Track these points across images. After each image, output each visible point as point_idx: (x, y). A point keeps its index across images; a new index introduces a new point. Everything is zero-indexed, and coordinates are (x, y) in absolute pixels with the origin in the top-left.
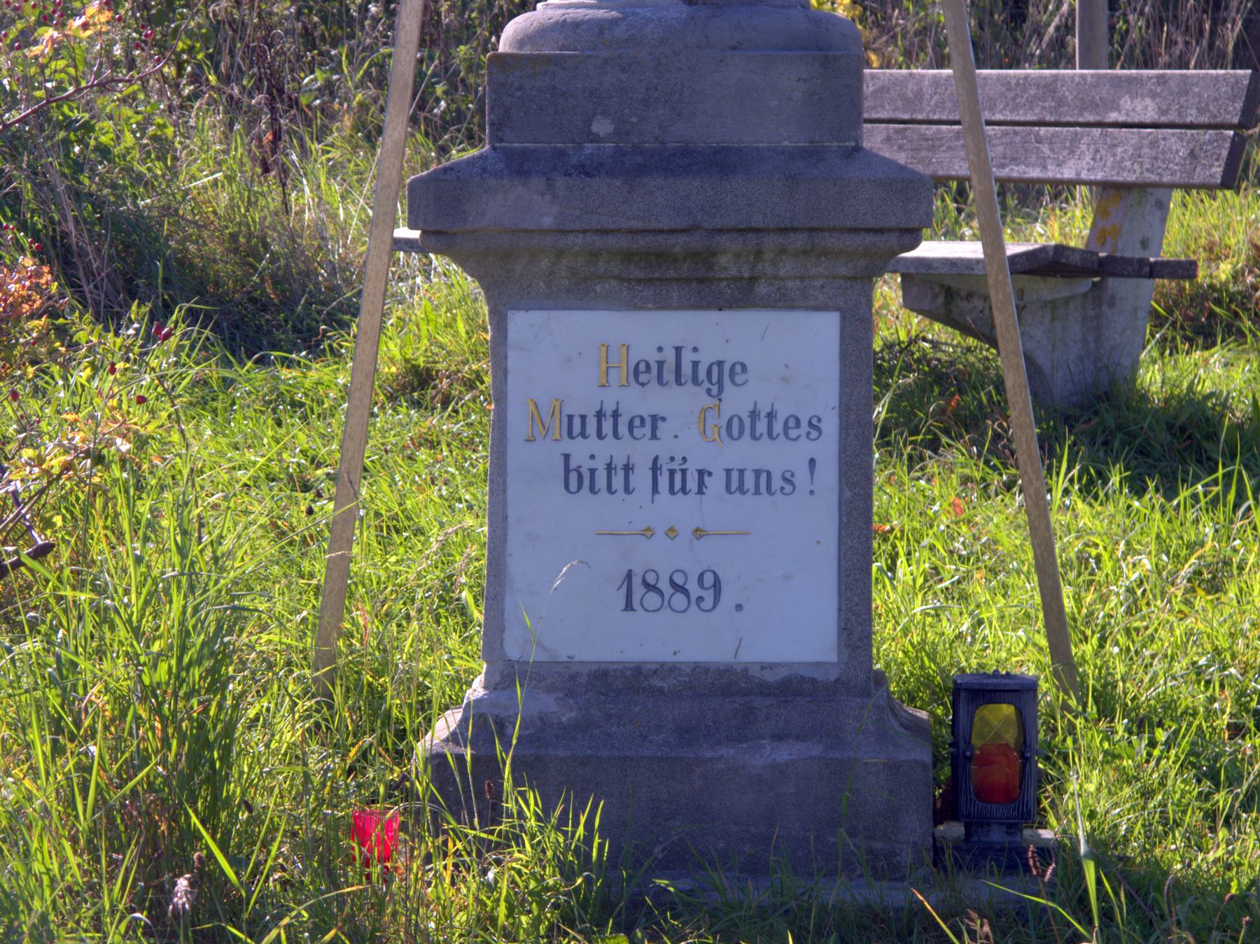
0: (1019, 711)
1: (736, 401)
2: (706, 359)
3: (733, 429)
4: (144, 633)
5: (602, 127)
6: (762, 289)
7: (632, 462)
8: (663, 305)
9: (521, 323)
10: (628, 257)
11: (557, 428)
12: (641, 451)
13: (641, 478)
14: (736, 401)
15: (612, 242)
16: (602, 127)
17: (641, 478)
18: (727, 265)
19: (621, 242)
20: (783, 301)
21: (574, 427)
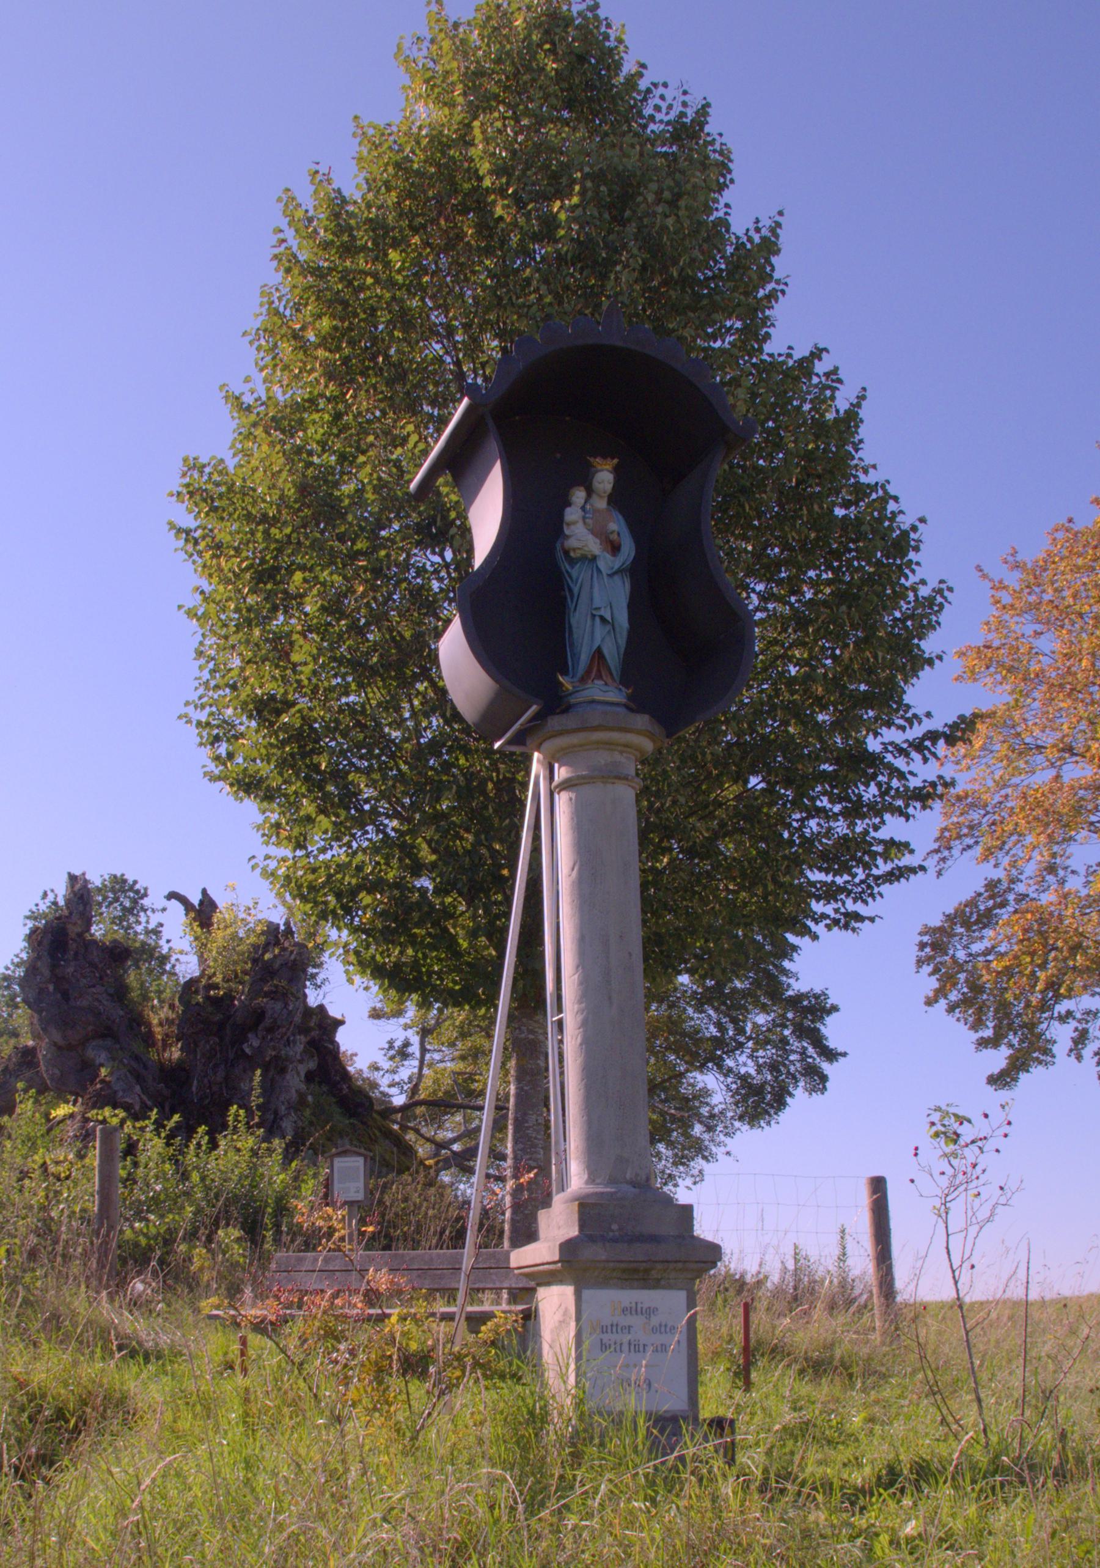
0: (433, 684)
1: (655, 1321)
2: (645, 1306)
3: (654, 1330)
4: (1076, 1029)
5: (615, 1227)
6: (663, 1282)
7: (841, 1059)
8: (632, 1288)
9: (587, 1294)
10: (624, 1271)
11: (598, 1330)
12: (626, 1338)
13: (625, 1347)
14: (655, 1321)
15: (623, 1265)
16: (615, 1227)
17: (625, 1347)
18: (654, 1274)
19: (623, 1265)
20: (669, 1287)
21: (604, 1330)
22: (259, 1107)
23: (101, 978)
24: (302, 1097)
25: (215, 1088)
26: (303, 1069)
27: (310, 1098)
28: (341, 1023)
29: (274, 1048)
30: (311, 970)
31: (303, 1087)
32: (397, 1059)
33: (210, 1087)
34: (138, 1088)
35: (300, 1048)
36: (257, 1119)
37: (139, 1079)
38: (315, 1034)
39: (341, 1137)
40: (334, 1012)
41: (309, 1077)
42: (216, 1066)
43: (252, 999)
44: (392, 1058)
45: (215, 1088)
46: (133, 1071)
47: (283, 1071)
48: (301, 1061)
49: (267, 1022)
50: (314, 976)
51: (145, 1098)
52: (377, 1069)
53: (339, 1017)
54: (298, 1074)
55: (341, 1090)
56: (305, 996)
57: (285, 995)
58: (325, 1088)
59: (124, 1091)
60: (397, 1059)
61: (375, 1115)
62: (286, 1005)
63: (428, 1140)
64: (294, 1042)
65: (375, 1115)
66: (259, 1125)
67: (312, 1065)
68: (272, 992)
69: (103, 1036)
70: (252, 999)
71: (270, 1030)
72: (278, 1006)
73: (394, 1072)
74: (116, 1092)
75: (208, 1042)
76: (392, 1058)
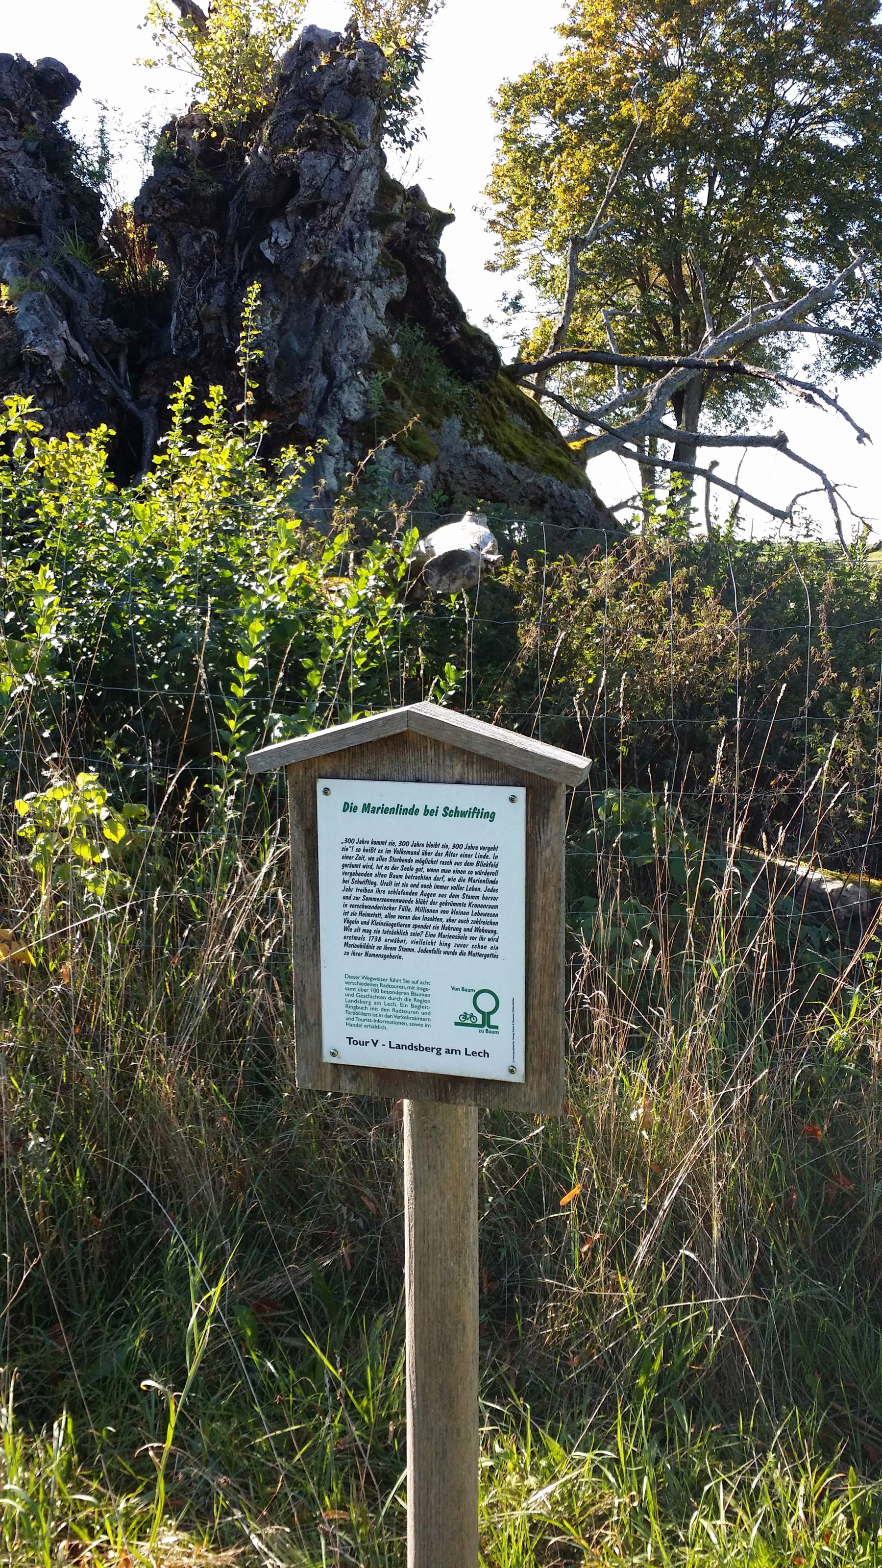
22: (257, 370)
23: (21, 125)
24: (380, 345)
25: (209, 328)
26: (382, 297)
27: (395, 349)
28: (449, 218)
29: (317, 248)
30: (395, 113)
31: (382, 329)
32: (510, 311)
33: (199, 326)
34: (63, 327)
35: (372, 254)
36: (249, 399)
37: (69, 312)
38: (400, 227)
39: (448, 415)
40: (436, 201)
41: (394, 309)
42: (211, 283)
43: (274, 152)
44: (506, 310)
45: (209, 328)
46: (56, 294)
47: (339, 295)
48: (377, 281)
49: (304, 195)
50: (398, 127)
51: (75, 345)
52: (491, 321)
53: (445, 210)
54: (374, 304)
55: (448, 334)
56: (383, 159)
57: (335, 140)
58: (420, 332)
59: (36, 332)
60: (510, 311)
61: (500, 376)
62: (339, 159)
63: (573, 411)
64: (362, 243)
65: (500, 376)
66: (255, 413)
67: (398, 289)
68: (310, 134)
69: (21, 232)
70: (274, 152)
71: (310, 211)
72: (324, 163)
73: (508, 323)
74: (22, 335)
75: (198, 238)
76: (506, 310)
